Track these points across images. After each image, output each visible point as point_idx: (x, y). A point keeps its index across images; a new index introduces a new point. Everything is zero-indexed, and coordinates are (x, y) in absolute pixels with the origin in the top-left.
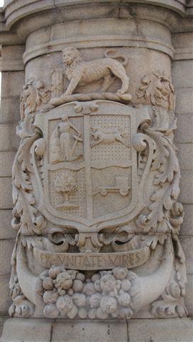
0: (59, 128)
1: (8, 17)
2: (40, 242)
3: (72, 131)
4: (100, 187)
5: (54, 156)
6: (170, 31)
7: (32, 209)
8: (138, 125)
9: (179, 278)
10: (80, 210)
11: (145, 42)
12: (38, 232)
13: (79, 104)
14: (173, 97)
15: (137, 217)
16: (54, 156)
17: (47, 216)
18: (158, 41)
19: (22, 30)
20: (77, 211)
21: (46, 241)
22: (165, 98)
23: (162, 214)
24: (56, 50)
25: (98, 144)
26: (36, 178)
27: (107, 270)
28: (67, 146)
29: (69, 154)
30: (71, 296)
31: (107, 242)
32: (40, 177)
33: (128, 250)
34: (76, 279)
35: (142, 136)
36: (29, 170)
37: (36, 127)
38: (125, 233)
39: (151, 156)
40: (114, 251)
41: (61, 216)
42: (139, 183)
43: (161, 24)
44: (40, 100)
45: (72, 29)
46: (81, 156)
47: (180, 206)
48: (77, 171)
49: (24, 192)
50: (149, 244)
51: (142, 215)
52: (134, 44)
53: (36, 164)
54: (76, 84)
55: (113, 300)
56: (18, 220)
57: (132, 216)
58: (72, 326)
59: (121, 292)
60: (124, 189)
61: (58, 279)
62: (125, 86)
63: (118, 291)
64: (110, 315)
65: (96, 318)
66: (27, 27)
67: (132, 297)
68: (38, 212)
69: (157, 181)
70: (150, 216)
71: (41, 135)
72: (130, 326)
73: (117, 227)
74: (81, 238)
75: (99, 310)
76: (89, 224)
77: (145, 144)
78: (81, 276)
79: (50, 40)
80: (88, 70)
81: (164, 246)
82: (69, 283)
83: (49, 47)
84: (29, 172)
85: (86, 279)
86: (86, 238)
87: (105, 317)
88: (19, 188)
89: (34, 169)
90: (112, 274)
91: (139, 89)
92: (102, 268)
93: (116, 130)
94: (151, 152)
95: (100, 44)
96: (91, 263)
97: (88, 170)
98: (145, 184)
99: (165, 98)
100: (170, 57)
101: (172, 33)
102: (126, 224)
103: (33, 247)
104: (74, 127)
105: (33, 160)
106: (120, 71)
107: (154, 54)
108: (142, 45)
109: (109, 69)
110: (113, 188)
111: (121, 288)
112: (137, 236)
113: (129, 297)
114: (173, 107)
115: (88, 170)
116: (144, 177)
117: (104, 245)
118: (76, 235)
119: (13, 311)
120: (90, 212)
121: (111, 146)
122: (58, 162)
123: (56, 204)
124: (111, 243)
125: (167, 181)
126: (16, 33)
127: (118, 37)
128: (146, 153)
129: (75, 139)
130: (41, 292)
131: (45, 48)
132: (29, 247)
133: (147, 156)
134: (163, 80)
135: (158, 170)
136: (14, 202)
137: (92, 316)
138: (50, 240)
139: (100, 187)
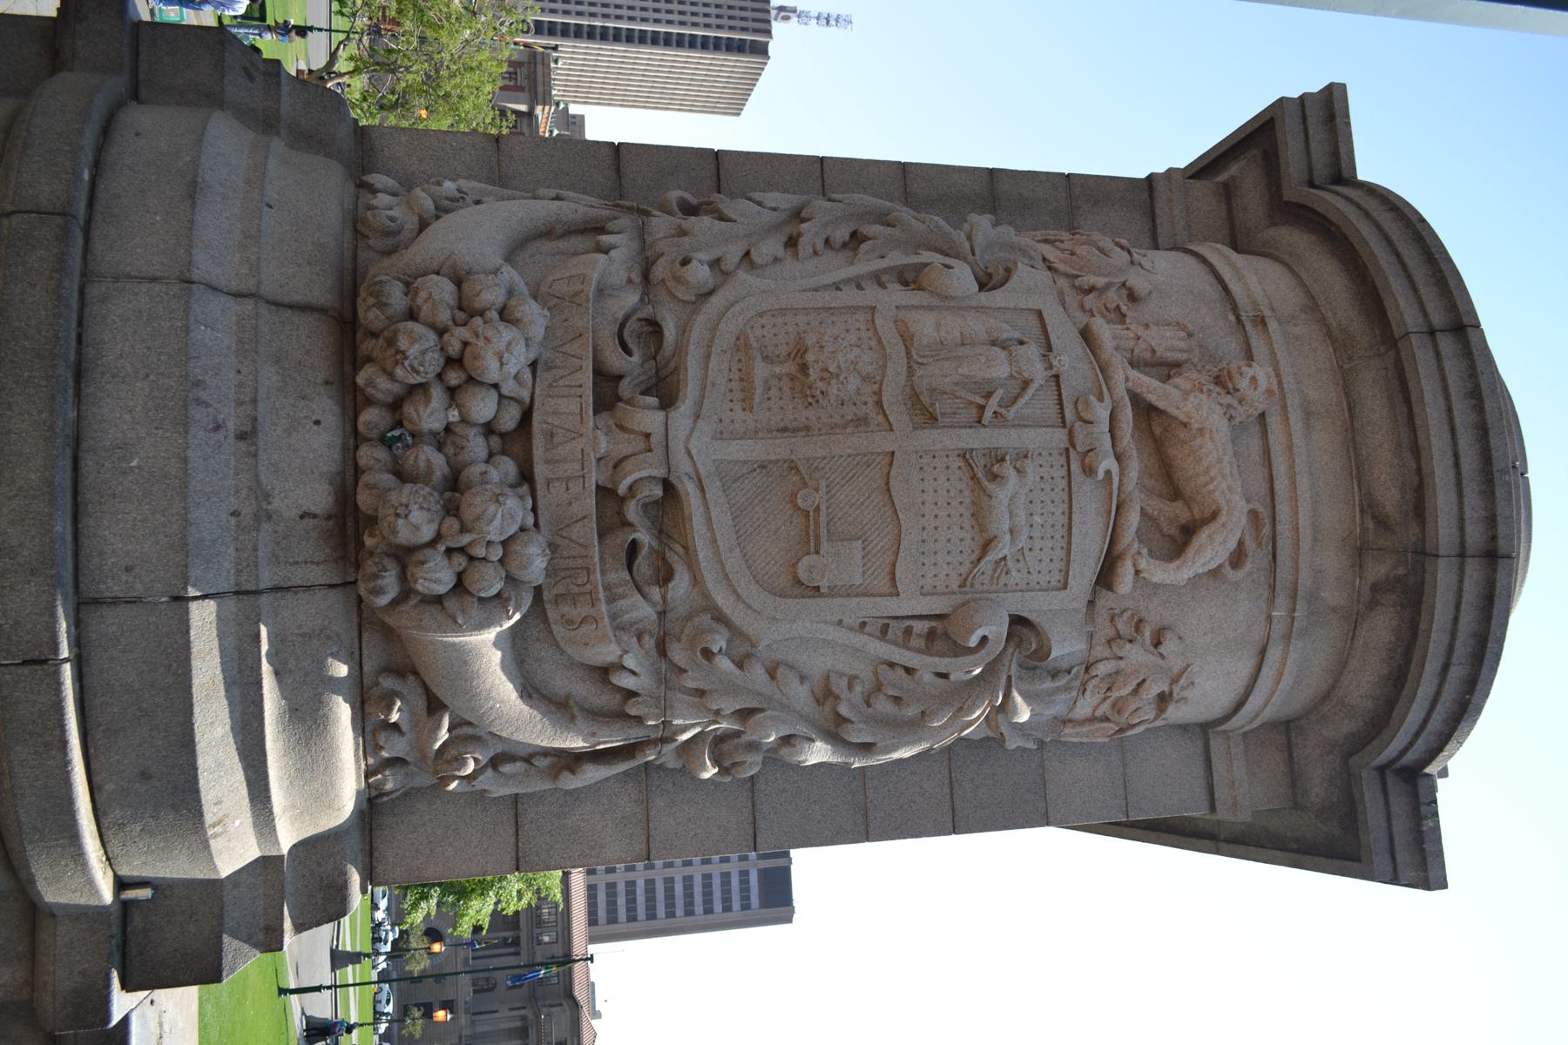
0: (1021, 343)
1: (1338, 194)
2: (624, 275)
3: (1014, 387)
4: (823, 483)
5: (926, 326)
6: (1298, 719)
7: (733, 253)
8: (1032, 617)
9: (507, 768)
10: (739, 415)
11: (1288, 637)
12: (659, 271)
13: (1102, 413)
14: (1100, 735)
15: (721, 618)
16: (926, 326)
17: (716, 302)
18: (1287, 679)
19: (1291, 237)
20: (737, 406)
21: (631, 298)
22: (1105, 708)
23: (729, 705)
24: (1254, 343)
25: (974, 477)
26: (838, 268)
27: (534, 509)
28: (964, 370)
29: (936, 375)
30: (440, 376)
31: (632, 511)
32: (848, 281)
33: (607, 588)
34: (501, 396)
35: (995, 628)
36: (864, 247)
37: (1009, 272)
38: (665, 576)
39: (926, 665)
40: (602, 535)
41: (716, 349)
42: (840, 622)
43: (1333, 687)
44: (1092, 289)
45: (1323, 392)
46: (931, 419)
47: (752, 765)
48: (879, 404)
49: (787, 230)
50: (630, 662)
51: (725, 632)
52: (1282, 601)
53: (885, 271)
54: (1161, 405)
55: (427, 533)
56: (690, 210)
57: (722, 599)
58: (327, 383)
59: (460, 561)
60: (821, 567)
61: (502, 326)
62: (1160, 573)
63: (462, 550)
64: (373, 521)
65: (358, 471)
66: (483, 637)
67: (438, 600)
68: (726, 274)
69: (839, 686)
70: (725, 664)
71: (985, 283)
72: (335, 596)
73: (686, 548)
74: (648, 418)
75: (387, 479)
76: (694, 445)
77: (973, 641)
78: (510, 419)
79: (1280, 323)
80: (1210, 446)
81: (620, 716)
82: (492, 371)
83: (1261, 322)
84: (855, 249)
85: (503, 435)
86: (648, 436)
87: (364, 499)
88: (797, 215)
89: (866, 264)
90: (523, 529)
91: (1141, 621)
92: (540, 493)
93: (1022, 541)
94: (942, 664)
95: (1281, 485)
96: (562, 451)
97: (884, 443)
98: (828, 643)
99: (1105, 708)
100: (1227, 718)
101: (1288, 722)
102: (696, 580)
103: (606, 252)
104: (1031, 391)
105: (896, 258)
106: (1208, 553)
107: (1244, 668)
108: (1278, 629)
109: (1214, 515)
110: (823, 532)
111: (472, 559)
112: (654, 617)
113: (442, 589)
114: (1070, 734)
115: (884, 443)
116: (858, 640)
117: (622, 500)
118: (652, 400)
119: (379, 186)
120: (737, 451)
121: (968, 522)
122: (907, 338)
123: (759, 332)
124: (630, 525)
125: (842, 720)
126: (1274, 224)
127: (1305, 546)
128: (939, 645)
129: (988, 395)
130: (454, 267)
131: (1255, 305)
132: (605, 239)
133: (927, 651)
134: (1163, 699)
135: (878, 687)
136: (757, 195)
137: (370, 455)
138: (634, 310)
139: (823, 483)
